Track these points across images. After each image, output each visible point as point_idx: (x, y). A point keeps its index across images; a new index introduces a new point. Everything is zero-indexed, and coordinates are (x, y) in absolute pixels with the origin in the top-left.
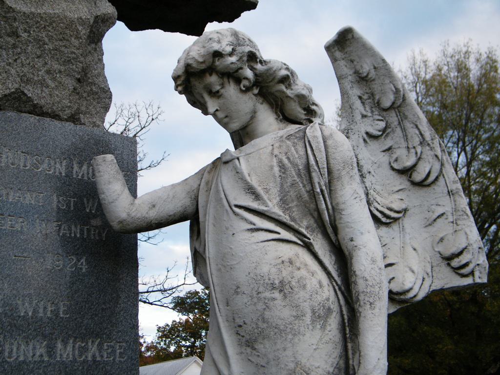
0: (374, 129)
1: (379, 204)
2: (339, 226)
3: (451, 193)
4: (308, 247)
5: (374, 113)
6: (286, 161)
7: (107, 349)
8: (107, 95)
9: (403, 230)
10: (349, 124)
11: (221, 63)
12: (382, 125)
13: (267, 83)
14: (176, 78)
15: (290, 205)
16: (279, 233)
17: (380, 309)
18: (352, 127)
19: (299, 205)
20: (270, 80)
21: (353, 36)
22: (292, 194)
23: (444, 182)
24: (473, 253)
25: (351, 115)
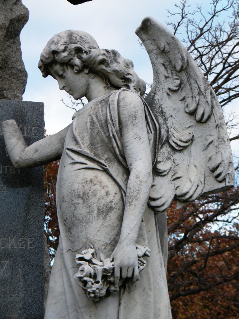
0: (173, 86)
1: (175, 138)
2: (126, 156)
3: (217, 126)
4: (106, 171)
5: (174, 74)
6: (95, 118)
7: (22, 241)
8: (24, 74)
9: (190, 153)
10: (156, 84)
11: (59, 58)
12: (178, 82)
13: (92, 65)
14: (40, 67)
15: (96, 146)
16: (87, 164)
17: (135, 206)
18: (158, 86)
19: (103, 146)
20: (93, 64)
21: (150, 23)
22: (98, 139)
23: (214, 120)
24: (224, 166)
25: (157, 78)
